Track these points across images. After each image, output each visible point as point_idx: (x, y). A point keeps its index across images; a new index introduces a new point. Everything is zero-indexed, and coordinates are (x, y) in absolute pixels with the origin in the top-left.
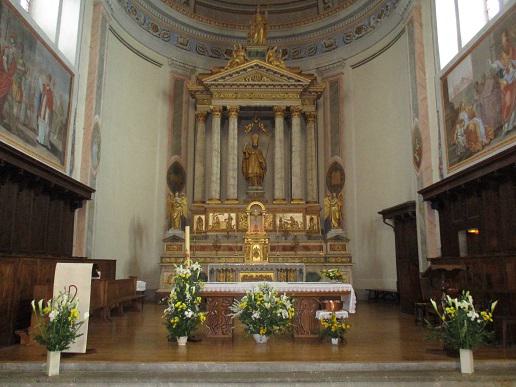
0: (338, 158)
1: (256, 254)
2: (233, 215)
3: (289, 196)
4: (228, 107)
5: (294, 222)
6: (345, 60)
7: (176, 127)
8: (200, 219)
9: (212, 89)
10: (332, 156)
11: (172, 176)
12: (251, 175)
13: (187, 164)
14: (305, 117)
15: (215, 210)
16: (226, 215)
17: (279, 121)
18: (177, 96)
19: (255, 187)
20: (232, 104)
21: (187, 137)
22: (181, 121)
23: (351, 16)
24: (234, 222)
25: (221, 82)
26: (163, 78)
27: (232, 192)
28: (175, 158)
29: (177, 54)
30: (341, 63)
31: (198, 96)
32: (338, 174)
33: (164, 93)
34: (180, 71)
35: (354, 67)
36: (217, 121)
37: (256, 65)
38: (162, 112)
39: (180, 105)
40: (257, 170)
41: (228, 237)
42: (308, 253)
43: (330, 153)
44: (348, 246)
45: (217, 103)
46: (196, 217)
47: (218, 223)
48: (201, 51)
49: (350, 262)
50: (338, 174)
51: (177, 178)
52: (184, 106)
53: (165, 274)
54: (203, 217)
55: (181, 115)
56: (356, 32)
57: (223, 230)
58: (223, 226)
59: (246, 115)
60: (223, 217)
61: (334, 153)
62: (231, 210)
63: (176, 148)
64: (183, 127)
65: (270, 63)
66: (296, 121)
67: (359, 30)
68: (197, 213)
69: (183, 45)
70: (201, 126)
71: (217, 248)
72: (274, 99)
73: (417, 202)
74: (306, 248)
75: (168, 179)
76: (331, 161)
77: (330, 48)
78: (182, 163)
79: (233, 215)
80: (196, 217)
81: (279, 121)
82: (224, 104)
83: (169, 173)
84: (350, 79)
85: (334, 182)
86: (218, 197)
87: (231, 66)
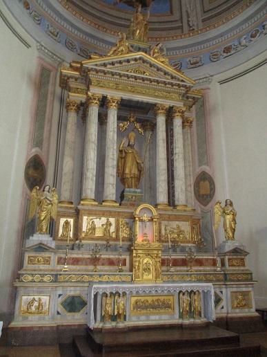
0: (205, 168)
1: (147, 270)
2: (112, 220)
3: (171, 202)
4: (109, 97)
5: (180, 232)
6: (212, 76)
7: (39, 115)
8: (67, 223)
9: (92, 75)
10: (199, 166)
11: (31, 171)
12: (128, 176)
13: (48, 158)
14: (186, 123)
15: (90, 213)
16: (104, 220)
17: (161, 121)
18: (41, 82)
19: (132, 190)
20: (115, 95)
21: (50, 130)
22: (45, 112)
23: (221, 35)
24: (112, 229)
25: (109, 68)
26: (30, 60)
27: (111, 191)
28: (35, 151)
29: (47, 41)
30: (208, 79)
31: (72, 84)
32: (207, 183)
33: (30, 77)
34: (48, 60)
35: (221, 82)
36: (94, 111)
37: (140, 58)
38: (25, 97)
39: (45, 96)
40: (135, 171)
41: (107, 247)
42: (201, 268)
43: (197, 163)
44: (247, 259)
45: (96, 91)
46: (63, 221)
47: (93, 229)
48: (70, 46)
49: (251, 280)
50: (207, 183)
51: (36, 173)
52: (50, 97)
53: (24, 298)
54: (71, 221)
55: (45, 106)
56: (224, 52)
57: (99, 239)
58: (99, 233)
59: (128, 108)
60: (99, 222)
61: (201, 163)
62: (110, 214)
63: (37, 141)
64: (46, 120)
65: (156, 58)
66: (178, 122)
67: (227, 50)
68: (64, 216)
69: (54, 35)
70: (72, 117)
71: (95, 261)
72: (157, 97)
73: (205, 208)
74: (199, 262)
75: (27, 174)
76: (198, 170)
77: (195, 65)
78: (43, 157)
79: (112, 220)
80: (63, 221)
81: (161, 121)
82: (105, 94)
83: (27, 168)
84: (216, 94)
85: (202, 192)
86: (93, 196)
87: (115, 53)
